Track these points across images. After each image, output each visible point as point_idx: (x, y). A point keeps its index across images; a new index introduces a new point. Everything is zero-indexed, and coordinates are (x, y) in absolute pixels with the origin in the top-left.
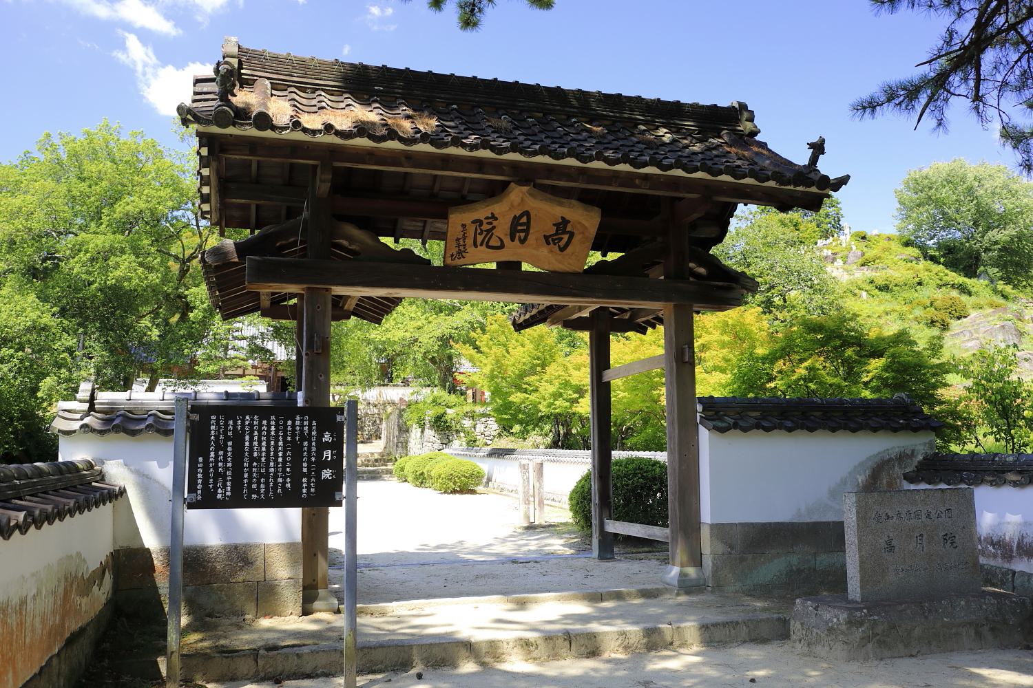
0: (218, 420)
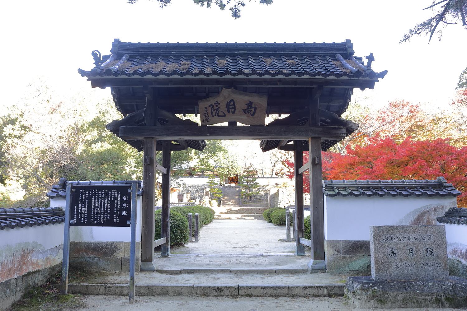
0: (82, 191)
